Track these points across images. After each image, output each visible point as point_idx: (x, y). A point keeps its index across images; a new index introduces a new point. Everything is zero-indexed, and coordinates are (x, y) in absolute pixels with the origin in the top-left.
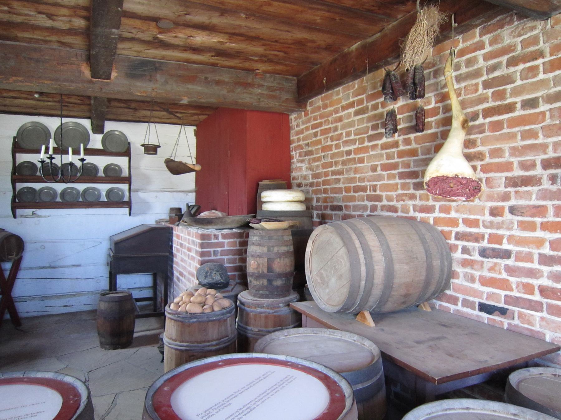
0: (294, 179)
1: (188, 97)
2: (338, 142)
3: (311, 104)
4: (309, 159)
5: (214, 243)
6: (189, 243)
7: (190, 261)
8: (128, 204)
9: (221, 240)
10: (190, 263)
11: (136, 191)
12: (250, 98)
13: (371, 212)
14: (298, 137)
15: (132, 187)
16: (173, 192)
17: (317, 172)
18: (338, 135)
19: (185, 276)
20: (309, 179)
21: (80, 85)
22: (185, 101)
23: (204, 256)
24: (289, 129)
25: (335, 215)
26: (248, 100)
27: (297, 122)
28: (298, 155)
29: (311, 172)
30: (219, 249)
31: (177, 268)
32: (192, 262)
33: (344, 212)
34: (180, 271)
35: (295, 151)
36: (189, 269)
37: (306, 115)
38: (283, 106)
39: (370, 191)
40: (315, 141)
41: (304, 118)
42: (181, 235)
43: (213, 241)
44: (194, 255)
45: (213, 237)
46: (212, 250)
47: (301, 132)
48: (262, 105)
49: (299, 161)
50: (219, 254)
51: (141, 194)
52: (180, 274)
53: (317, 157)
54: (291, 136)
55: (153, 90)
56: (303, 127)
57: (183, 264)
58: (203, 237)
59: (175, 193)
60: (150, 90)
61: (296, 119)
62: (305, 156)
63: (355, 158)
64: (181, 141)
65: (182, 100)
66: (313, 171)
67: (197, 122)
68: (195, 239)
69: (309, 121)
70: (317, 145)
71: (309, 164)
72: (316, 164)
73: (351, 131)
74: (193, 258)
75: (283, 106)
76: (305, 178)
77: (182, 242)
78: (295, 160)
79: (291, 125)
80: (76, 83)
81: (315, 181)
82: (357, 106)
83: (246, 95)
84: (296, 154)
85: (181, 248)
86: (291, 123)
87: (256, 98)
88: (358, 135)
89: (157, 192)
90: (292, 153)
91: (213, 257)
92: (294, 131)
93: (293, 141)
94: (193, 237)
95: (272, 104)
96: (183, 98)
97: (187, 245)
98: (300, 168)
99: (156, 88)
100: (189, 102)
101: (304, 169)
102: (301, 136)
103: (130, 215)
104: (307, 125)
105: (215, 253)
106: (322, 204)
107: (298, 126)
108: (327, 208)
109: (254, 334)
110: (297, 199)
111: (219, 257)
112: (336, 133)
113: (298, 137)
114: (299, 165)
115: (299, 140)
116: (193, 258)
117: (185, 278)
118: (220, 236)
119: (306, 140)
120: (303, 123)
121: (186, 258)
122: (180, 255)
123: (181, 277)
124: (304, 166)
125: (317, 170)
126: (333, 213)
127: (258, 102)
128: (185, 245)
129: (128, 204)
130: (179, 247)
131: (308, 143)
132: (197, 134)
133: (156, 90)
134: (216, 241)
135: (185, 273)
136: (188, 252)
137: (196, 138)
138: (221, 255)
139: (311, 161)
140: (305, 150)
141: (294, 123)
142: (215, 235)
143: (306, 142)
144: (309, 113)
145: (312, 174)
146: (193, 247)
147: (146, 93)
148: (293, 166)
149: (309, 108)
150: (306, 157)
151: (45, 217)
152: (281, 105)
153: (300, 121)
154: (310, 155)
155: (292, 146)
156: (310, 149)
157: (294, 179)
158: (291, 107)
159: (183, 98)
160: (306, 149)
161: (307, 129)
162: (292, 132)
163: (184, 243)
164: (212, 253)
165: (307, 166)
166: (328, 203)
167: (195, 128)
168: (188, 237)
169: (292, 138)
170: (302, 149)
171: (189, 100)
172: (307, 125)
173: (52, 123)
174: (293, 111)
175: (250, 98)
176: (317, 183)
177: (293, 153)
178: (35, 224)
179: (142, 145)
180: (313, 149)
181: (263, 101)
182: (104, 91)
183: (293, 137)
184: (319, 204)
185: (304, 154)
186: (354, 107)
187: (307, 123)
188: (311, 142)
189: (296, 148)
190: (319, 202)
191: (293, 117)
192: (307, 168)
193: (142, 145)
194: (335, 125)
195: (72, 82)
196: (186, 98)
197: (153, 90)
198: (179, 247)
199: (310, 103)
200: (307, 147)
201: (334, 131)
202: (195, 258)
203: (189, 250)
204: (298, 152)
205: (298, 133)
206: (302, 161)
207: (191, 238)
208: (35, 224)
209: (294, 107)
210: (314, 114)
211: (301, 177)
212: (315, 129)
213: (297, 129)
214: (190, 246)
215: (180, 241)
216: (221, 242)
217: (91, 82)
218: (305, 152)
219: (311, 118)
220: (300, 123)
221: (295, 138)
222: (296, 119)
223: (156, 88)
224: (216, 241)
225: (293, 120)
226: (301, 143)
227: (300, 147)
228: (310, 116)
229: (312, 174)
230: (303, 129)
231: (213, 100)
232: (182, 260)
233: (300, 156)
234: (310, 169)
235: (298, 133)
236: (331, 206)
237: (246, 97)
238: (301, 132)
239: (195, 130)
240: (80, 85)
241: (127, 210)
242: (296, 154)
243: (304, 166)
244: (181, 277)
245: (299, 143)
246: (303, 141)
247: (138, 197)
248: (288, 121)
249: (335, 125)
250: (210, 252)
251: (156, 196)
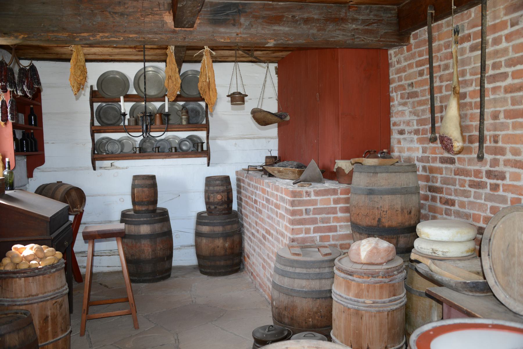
0: (395, 124)
1: (275, 40)
2: (449, 82)
3: (416, 37)
4: (413, 102)
5: (306, 200)
6: (277, 200)
7: (278, 219)
8: (207, 154)
9: (313, 197)
10: (279, 221)
11: (215, 139)
12: (343, 35)
13: (491, 166)
14: (399, 75)
15: (211, 135)
16: (254, 138)
17: (423, 117)
18: (449, 74)
19: (272, 234)
20: (413, 125)
21: (163, 36)
22: (271, 43)
23: (296, 215)
24: (387, 66)
25: (446, 168)
26: (340, 38)
27: (396, 57)
28: (399, 96)
29: (416, 118)
30: (311, 208)
31: (246, 219)
32: (281, 220)
33: (457, 165)
34: (266, 229)
35: (396, 92)
36: (278, 228)
37: (409, 50)
38: (381, 41)
39: (490, 142)
40: (421, 81)
41: (406, 54)
42: (268, 189)
43: (304, 198)
44: (284, 213)
45: (305, 194)
46: (303, 208)
47: (404, 70)
48: (357, 42)
49: (400, 104)
50: (311, 213)
51: (219, 142)
52: (266, 232)
53: (423, 100)
54: (390, 74)
55: (237, 35)
56: (406, 64)
57: (270, 222)
58: (294, 194)
59: (256, 140)
60: (234, 35)
61: (396, 54)
62: (408, 98)
63: (471, 103)
64: (261, 82)
65: (267, 43)
66: (418, 116)
67: (279, 59)
68: (284, 196)
69: (413, 56)
70: (422, 86)
71: (414, 107)
72: (422, 108)
73: (466, 70)
74: (282, 217)
75: (381, 41)
76: (408, 123)
77: (269, 198)
78: (396, 102)
79: (390, 61)
80: (160, 34)
81: (421, 128)
82: (474, 40)
83: (338, 32)
84: (397, 95)
85: (267, 204)
86: (391, 59)
87: (350, 34)
88: (474, 75)
89: (236, 139)
90: (391, 95)
91: (305, 216)
92: (394, 68)
93: (394, 81)
94: (282, 193)
95: (369, 40)
96: (269, 41)
97: (275, 201)
98: (403, 113)
99: (240, 33)
100: (275, 44)
101: (407, 113)
102: (403, 74)
103: (208, 165)
104: (410, 62)
105: (307, 212)
106: (430, 155)
107: (398, 62)
108: (436, 160)
109: (368, 307)
110: (474, 270)
111: (312, 216)
112: (447, 72)
113: (399, 75)
114: (400, 108)
115: (400, 79)
116: (282, 217)
117: (272, 237)
118: (312, 193)
119: (410, 80)
120: (406, 60)
121: (274, 216)
122: (266, 211)
123: (267, 236)
124: (407, 109)
125: (422, 115)
126: (444, 166)
127: (352, 39)
128: (272, 201)
129: (207, 154)
130: (264, 202)
131: (412, 83)
132: (278, 71)
133: (240, 35)
134: (308, 198)
135: (272, 231)
136: (276, 209)
137: (279, 79)
138: (314, 214)
139: (416, 104)
140: (407, 91)
141: (393, 60)
142: (307, 192)
143: (409, 82)
144: (413, 47)
145: (417, 120)
146: (282, 204)
147: (230, 39)
148: (394, 110)
149: (412, 41)
150: (410, 100)
151: (123, 168)
152: (379, 41)
153: (402, 57)
154: (415, 97)
155: (391, 86)
156: (415, 89)
157: (395, 124)
158: (392, 42)
159: (269, 41)
160: (409, 90)
161: (410, 66)
162: (392, 70)
163: (271, 199)
164: (304, 211)
165: (411, 110)
166: (436, 154)
167: (276, 65)
168: (276, 193)
169: (391, 77)
170: (404, 89)
171: (275, 42)
172: (410, 62)
173: (130, 70)
174: (392, 46)
175: (343, 35)
176: (423, 130)
177: (393, 95)
178: (114, 176)
179: (228, 96)
180: (418, 89)
181: (358, 38)
182: (187, 40)
183: (393, 76)
184: (426, 155)
185: (406, 96)
186: (470, 41)
187: (410, 60)
188: (416, 82)
189: (396, 89)
190: (426, 153)
191: (391, 52)
192: (410, 112)
193: (228, 96)
194: (446, 62)
195: (156, 33)
196: (272, 41)
197: (237, 35)
198: (264, 202)
199: (413, 35)
200: (410, 88)
201: (444, 70)
202: (284, 216)
203: (277, 206)
204: (399, 93)
205: (398, 71)
206: (405, 104)
207: (279, 194)
208: (114, 176)
209: (394, 42)
210: (418, 49)
211: (404, 122)
212: (421, 66)
213: (397, 66)
214: (278, 202)
215: (266, 196)
216: (313, 200)
217: (174, 32)
218: (408, 93)
219: (415, 53)
220: (402, 59)
221: (396, 76)
222: (396, 54)
223: (240, 33)
224: (308, 198)
225: (393, 56)
226: (403, 82)
227: (402, 87)
228: (413, 51)
229: (417, 120)
230: (405, 67)
231: (301, 41)
232: (269, 217)
233: (402, 98)
234: (415, 113)
235: (398, 71)
236: (440, 158)
237: (337, 34)
238: (404, 70)
239: (276, 68)
240: (163, 36)
241: (205, 160)
242: (397, 95)
243: (407, 109)
244: (267, 236)
245: (400, 83)
246: (406, 80)
247: (214, 146)
248: (386, 57)
249: (446, 62)
250: (301, 211)
251: (236, 144)
